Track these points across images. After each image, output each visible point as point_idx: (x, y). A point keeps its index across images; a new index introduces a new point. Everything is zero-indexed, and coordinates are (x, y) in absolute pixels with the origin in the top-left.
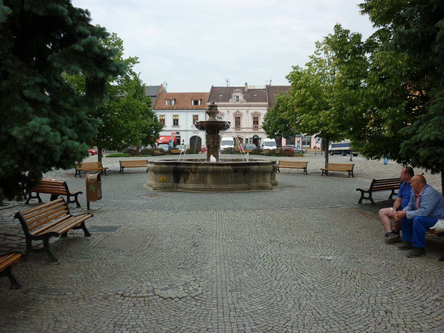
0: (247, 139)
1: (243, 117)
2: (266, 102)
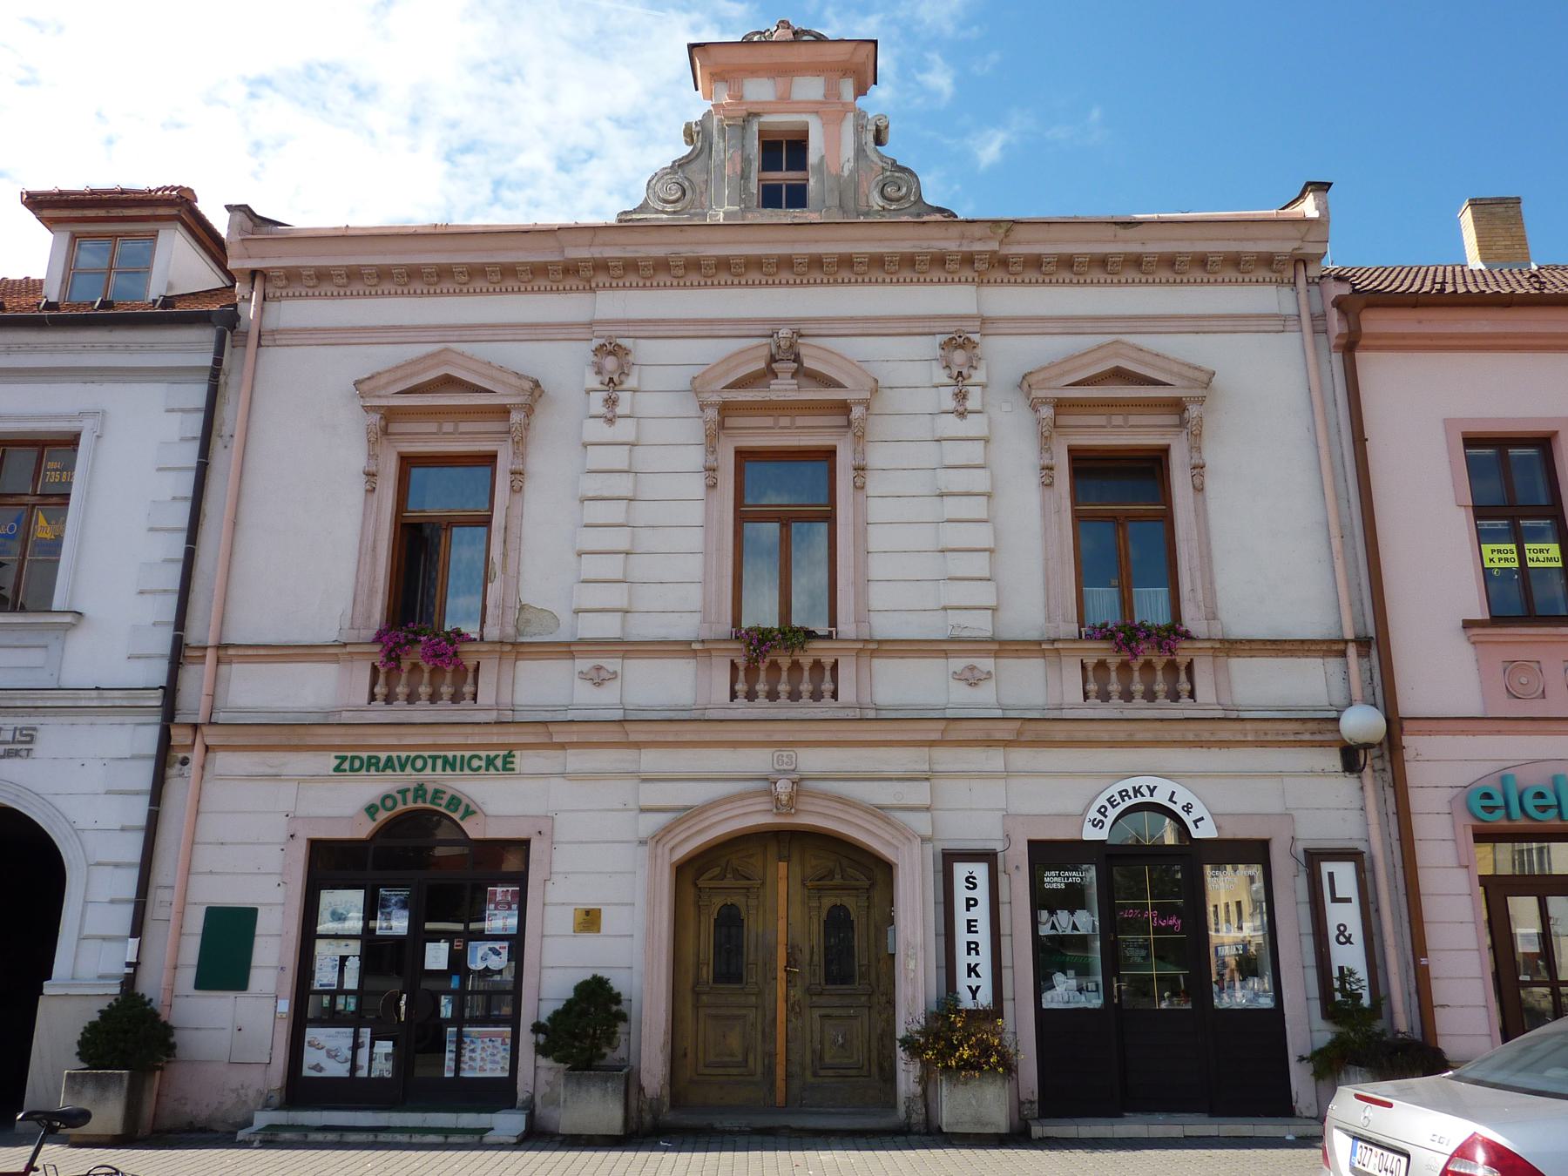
1: (877, 456)
2: (724, 219)
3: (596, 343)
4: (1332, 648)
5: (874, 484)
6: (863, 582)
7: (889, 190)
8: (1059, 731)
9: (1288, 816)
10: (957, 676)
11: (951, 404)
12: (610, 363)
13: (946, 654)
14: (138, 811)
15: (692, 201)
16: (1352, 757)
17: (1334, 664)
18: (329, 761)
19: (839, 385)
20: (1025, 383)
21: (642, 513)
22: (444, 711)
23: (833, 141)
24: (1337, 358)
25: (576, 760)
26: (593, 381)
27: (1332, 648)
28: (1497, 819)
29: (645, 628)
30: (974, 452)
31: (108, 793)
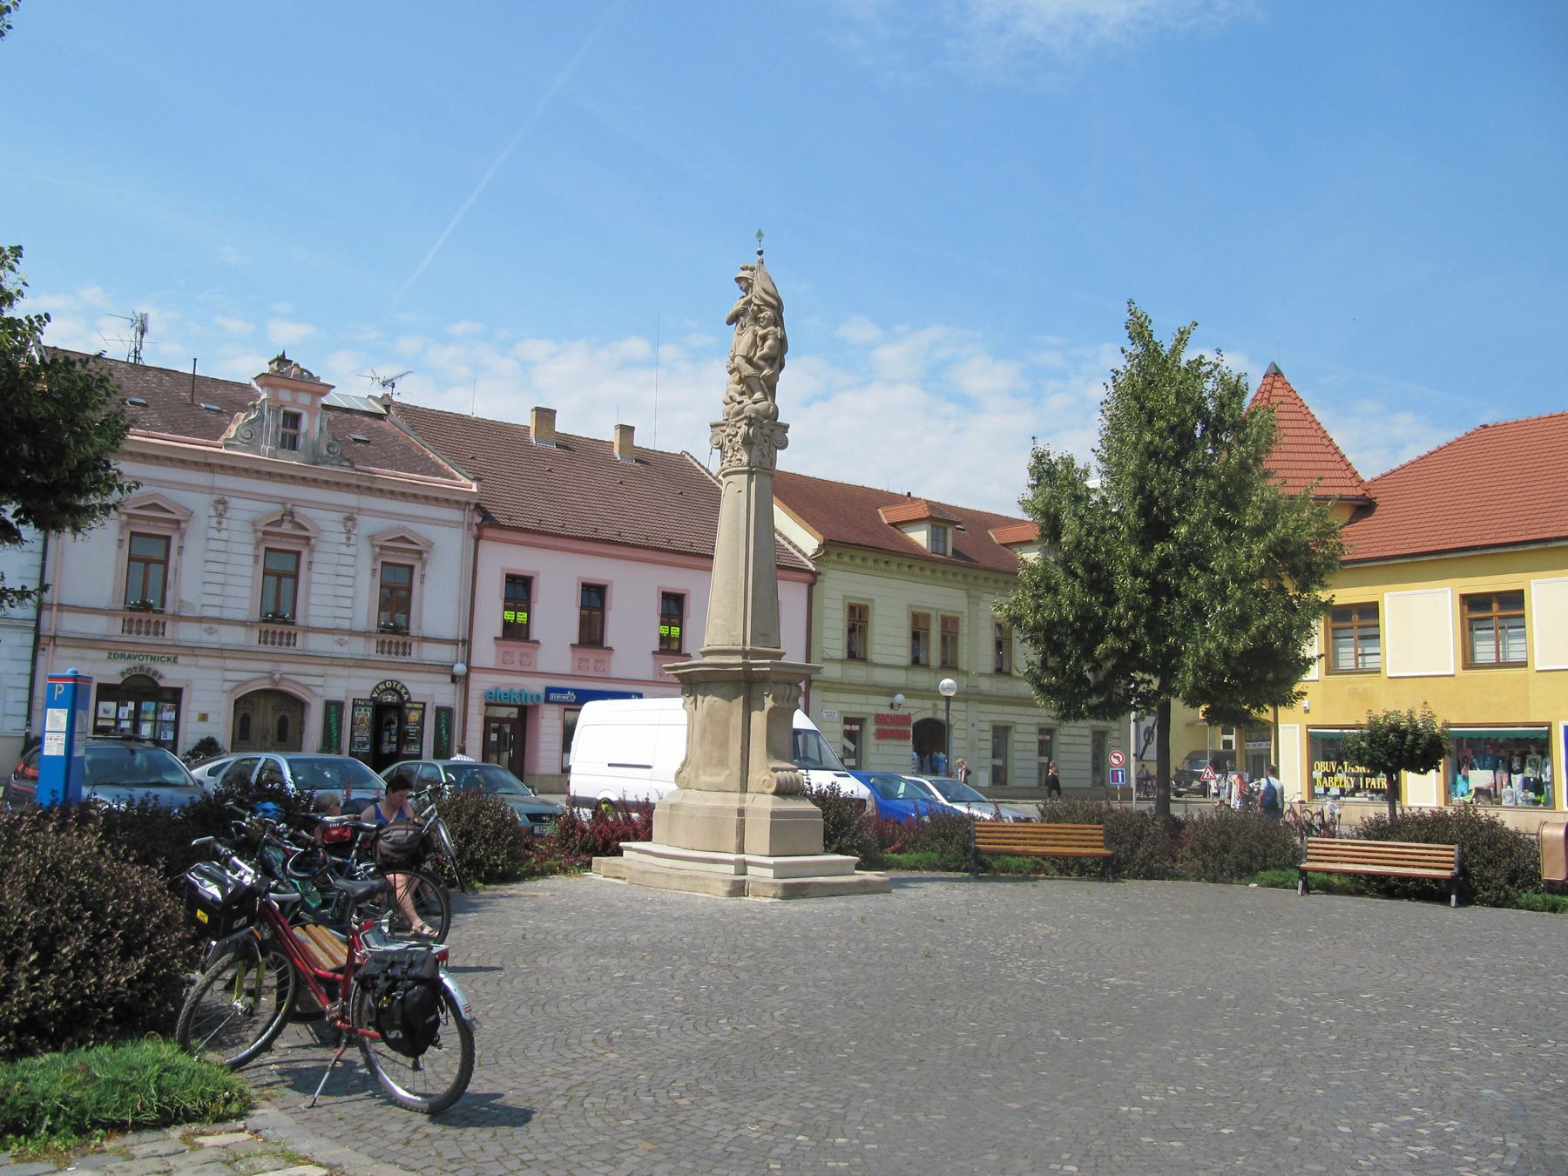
0: (340, 705)
1: (317, 557)
3: (215, 497)
4: (455, 642)
5: (315, 568)
6: (307, 604)
7: (331, 449)
8: (368, 664)
9: (432, 696)
10: (337, 642)
11: (344, 541)
12: (221, 507)
13: (333, 634)
14: (27, 668)
15: (255, 441)
16: (454, 679)
17: (454, 647)
18: (105, 655)
19: (306, 530)
20: (371, 538)
21: (230, 569)
22: (151, 639)
23: (311, 423)
24: (473, 541)
25: (202, 661)
26: (212, 512)
27: (455, 642)
28: (492, 701)
29: (228, 614)
30: (350, 560)
31: (12, 659)
